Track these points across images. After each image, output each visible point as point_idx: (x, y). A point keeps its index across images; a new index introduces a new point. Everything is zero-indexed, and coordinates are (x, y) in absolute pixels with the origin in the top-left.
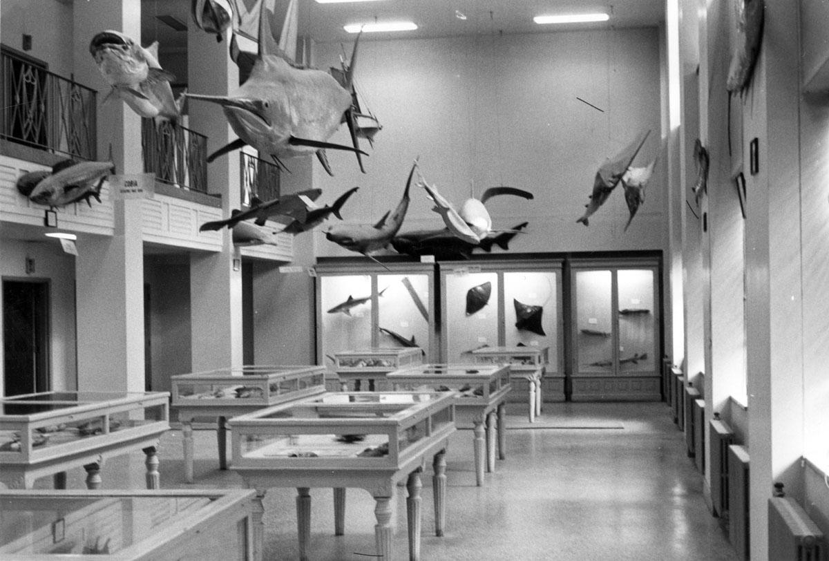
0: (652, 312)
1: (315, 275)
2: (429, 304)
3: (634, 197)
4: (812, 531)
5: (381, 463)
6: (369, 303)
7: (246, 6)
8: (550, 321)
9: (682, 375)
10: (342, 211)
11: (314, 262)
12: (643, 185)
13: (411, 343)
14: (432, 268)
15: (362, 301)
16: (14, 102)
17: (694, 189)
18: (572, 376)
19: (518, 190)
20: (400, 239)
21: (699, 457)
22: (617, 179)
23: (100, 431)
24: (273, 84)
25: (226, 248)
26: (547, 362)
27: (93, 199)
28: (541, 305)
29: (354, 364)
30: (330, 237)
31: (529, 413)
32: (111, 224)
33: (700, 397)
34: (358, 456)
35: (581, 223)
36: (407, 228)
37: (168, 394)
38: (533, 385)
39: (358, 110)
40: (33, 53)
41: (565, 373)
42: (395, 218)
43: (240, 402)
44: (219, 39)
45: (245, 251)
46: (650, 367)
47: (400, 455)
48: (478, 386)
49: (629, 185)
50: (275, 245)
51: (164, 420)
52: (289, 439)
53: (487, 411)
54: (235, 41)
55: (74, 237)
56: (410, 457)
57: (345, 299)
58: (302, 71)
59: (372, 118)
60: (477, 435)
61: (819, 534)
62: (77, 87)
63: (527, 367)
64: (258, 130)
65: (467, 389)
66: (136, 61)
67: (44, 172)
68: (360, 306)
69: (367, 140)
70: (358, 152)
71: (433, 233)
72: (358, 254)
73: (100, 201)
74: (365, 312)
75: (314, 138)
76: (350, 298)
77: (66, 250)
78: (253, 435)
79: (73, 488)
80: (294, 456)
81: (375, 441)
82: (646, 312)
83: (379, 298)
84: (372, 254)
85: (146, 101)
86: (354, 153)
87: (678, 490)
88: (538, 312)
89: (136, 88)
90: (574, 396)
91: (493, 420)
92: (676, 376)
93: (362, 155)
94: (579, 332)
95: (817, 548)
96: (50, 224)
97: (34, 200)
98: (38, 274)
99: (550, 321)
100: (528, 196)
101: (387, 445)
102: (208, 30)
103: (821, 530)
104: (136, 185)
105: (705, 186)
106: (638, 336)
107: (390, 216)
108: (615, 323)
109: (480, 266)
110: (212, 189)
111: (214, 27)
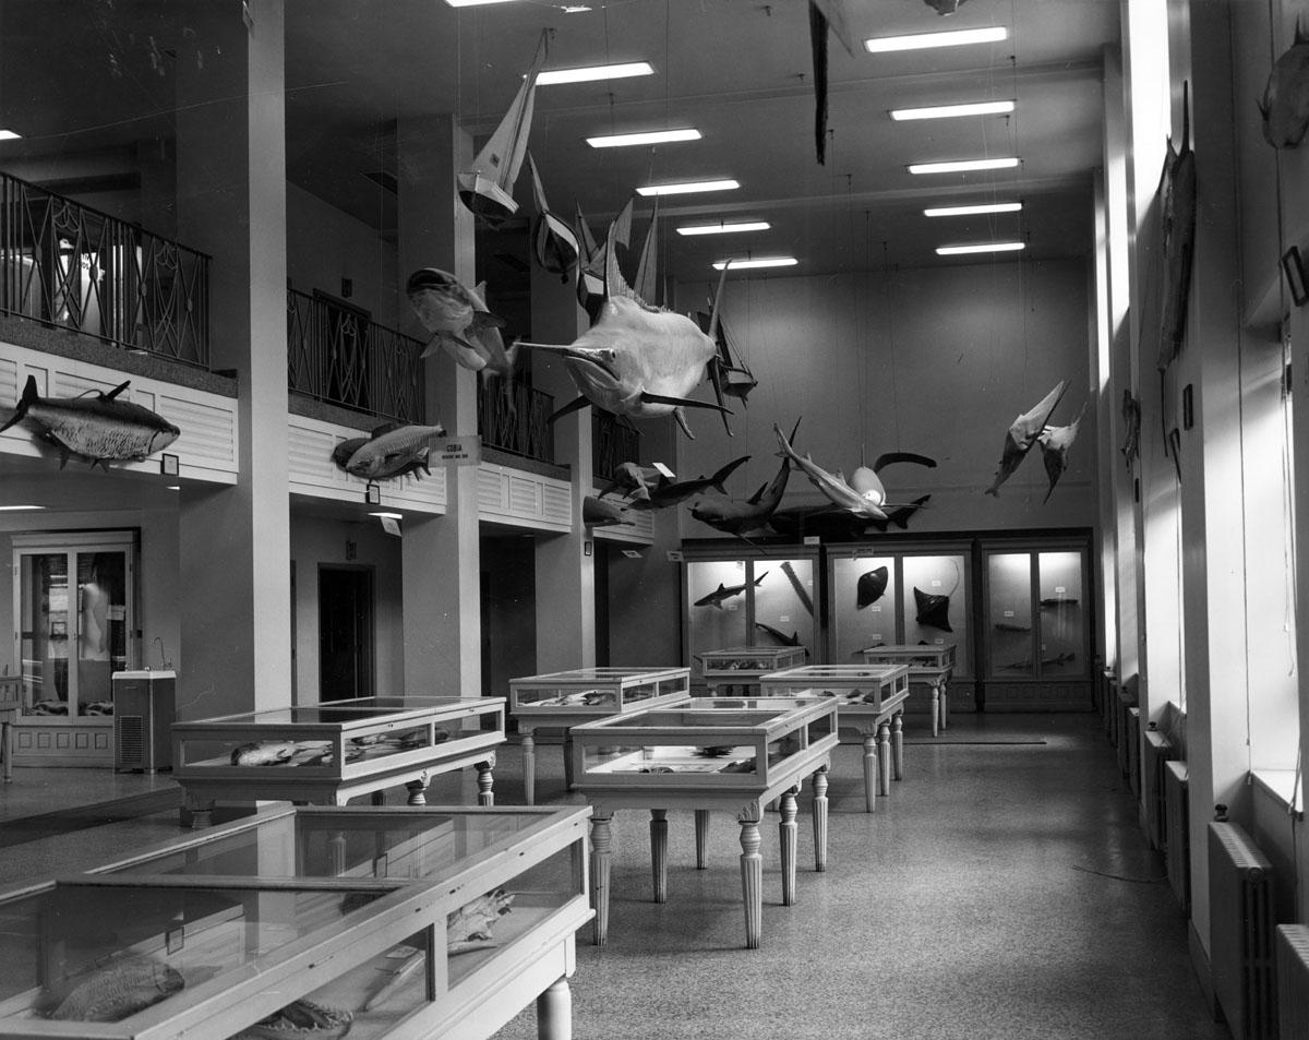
0: (1080, 603)
1: (681, 559)
2: (814, 593)
3: (1053, 458)
4: (1259, 862)
5: (745, 782)
6: (743, 593)
7: (596, 241)
8: (957, 613)
9: (1115, 679)
10: (725, 484)
11: (679, 544)
12: (1066, 447)
13: (793, 642)
14: (817, 550)
15: (736, 591)
16: (330, 357)
17: (1124, 451)
18: (985, 681)
19: (910, 455)
20: (780, 517)
21: (1133, 780)
22: (1031, 440)
23: (425, 743)
24: (620, 330)
25: (575, 527)
26: (954, 665)
27: (422, 471)
28: (946, 595)
29: (726, 666)
30: (696, 515)
31: (932, 728)
32: (444, 501)
33: (1135, 705)
34: (721, 771)
35: (991, 494)
36: (785, 504)
37: (504, 699)
38: (936, 692)
39: (728, 362)
40: (354, 300)
41: (976, 678)
42: (773, 491)
43: (589, 711)
44: (565, 280)
45: (598, 532)
46: (1078, 670)
47: (770, 772)
48: (868, 692)
49: (1049, 447)
50: (633, 524)
51: (499, 730)
52: (641, 752)
53: (879, 721)
54: (584, 283)
55: (400, 517)
56: (788, 775)
57: (715, 589)
58: (658, 315)
59: (745, 372)
60: (867, 750)
61: (1269, 866)
62: (403, 339)
63: (929, 670)
64: (604, 386)
65: (856, 694)
66: (459, 304)
67: (365, 439)
68: (734, 597)
69: (739, 399)
70: (723, 411)
71: (817, 509)
72: (732, 536)
73: (429, 474)
74: (739, 604)
75: (671, 394)
76: (722, 585)
77: (387, 530)
78: (605, 745)
79: (392, 804)
80: (646, 771)
81: (742, 755)
82: (1075, 602)
83: (756, 588)
84: (746, 535)
85: (472, 350)
86: (719, 412)
87: (1112, 817)
88: (943, 603)
89: (460, 335)
90: (988, 704)
91: (887, 732)
92: (1109, 679)
93: (727, 414)
94: (993, 627)
95: (1265, 883)
96: (371, 501)
97: (349, 471)
98: (362, 559)
99: (957, 613)
100: (931, 463)
101: (753, 759)
102: (552, 269)
103: (1271, 862)
104: (460, 449)
105: (1137, 448)
106: (1062, 628)
107: (766, 489)
108: (1036, 616)
109: (873, 549)
110: (558, 461)
111: (557, 264)
